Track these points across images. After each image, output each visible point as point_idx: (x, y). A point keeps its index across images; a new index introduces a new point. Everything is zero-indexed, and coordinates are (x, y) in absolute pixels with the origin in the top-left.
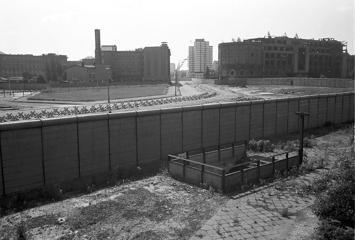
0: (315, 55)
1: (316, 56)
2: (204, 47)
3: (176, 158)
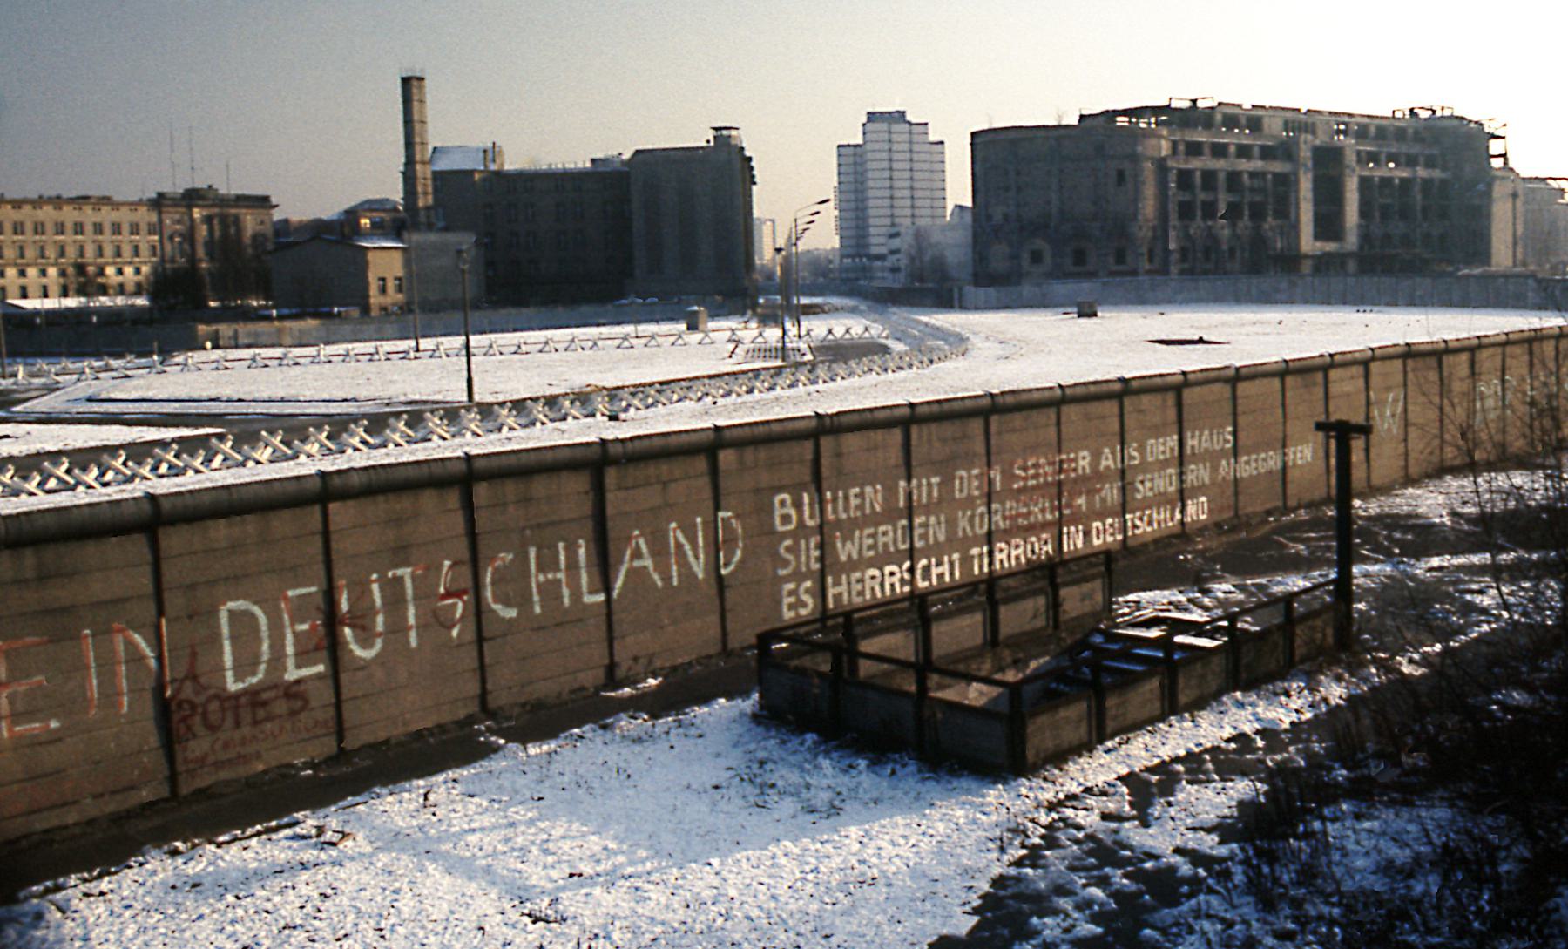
0: (1382, 179)
1: (1386, 182)
2: (907, 184)
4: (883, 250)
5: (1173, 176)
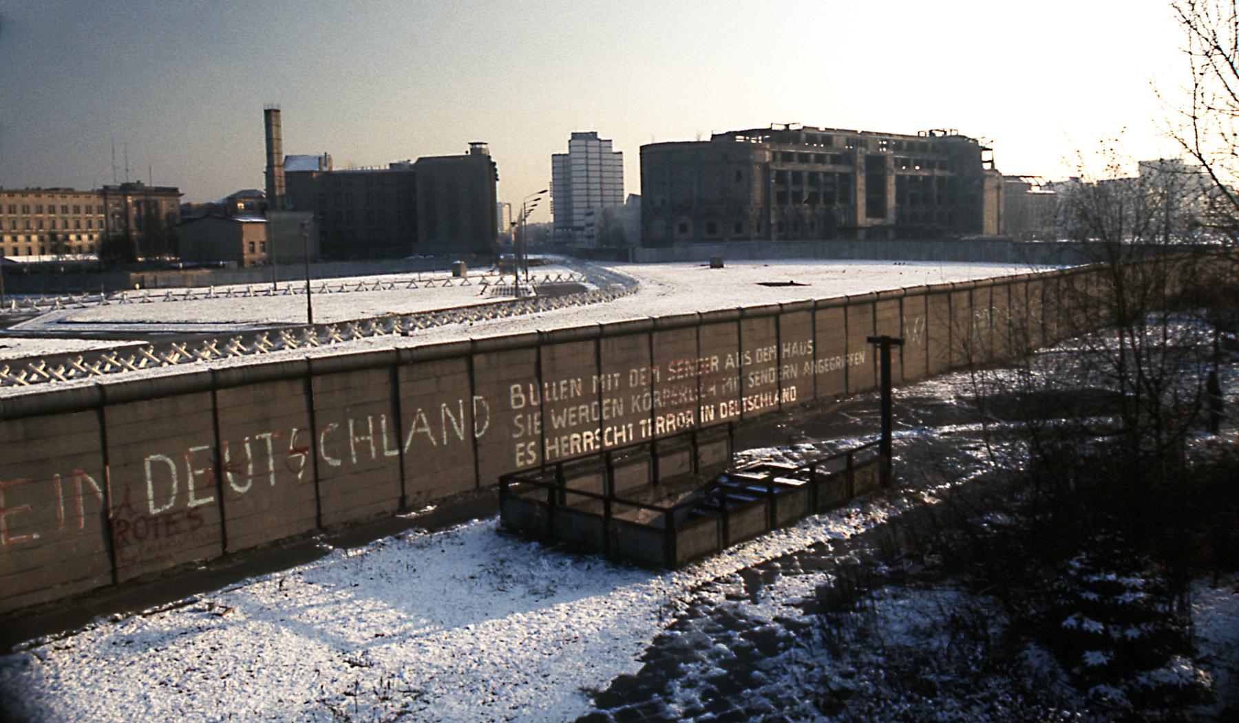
0: (911, 177)
1: (914, 179)
3: (459, 426)
4: (582, 224)
5: (773, 175)
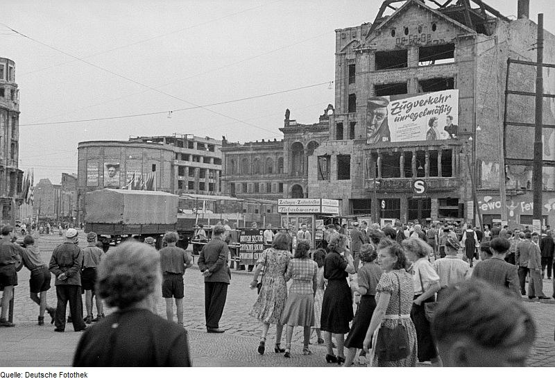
5: (176, 168)
